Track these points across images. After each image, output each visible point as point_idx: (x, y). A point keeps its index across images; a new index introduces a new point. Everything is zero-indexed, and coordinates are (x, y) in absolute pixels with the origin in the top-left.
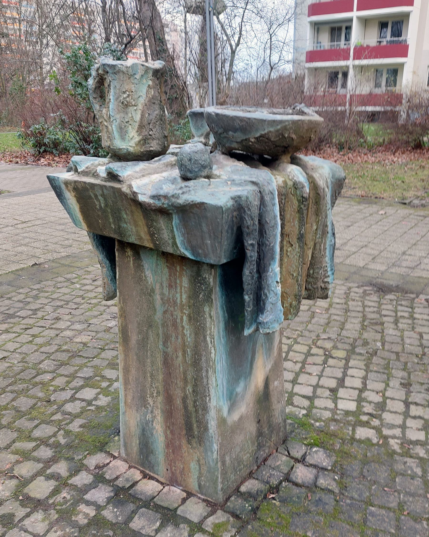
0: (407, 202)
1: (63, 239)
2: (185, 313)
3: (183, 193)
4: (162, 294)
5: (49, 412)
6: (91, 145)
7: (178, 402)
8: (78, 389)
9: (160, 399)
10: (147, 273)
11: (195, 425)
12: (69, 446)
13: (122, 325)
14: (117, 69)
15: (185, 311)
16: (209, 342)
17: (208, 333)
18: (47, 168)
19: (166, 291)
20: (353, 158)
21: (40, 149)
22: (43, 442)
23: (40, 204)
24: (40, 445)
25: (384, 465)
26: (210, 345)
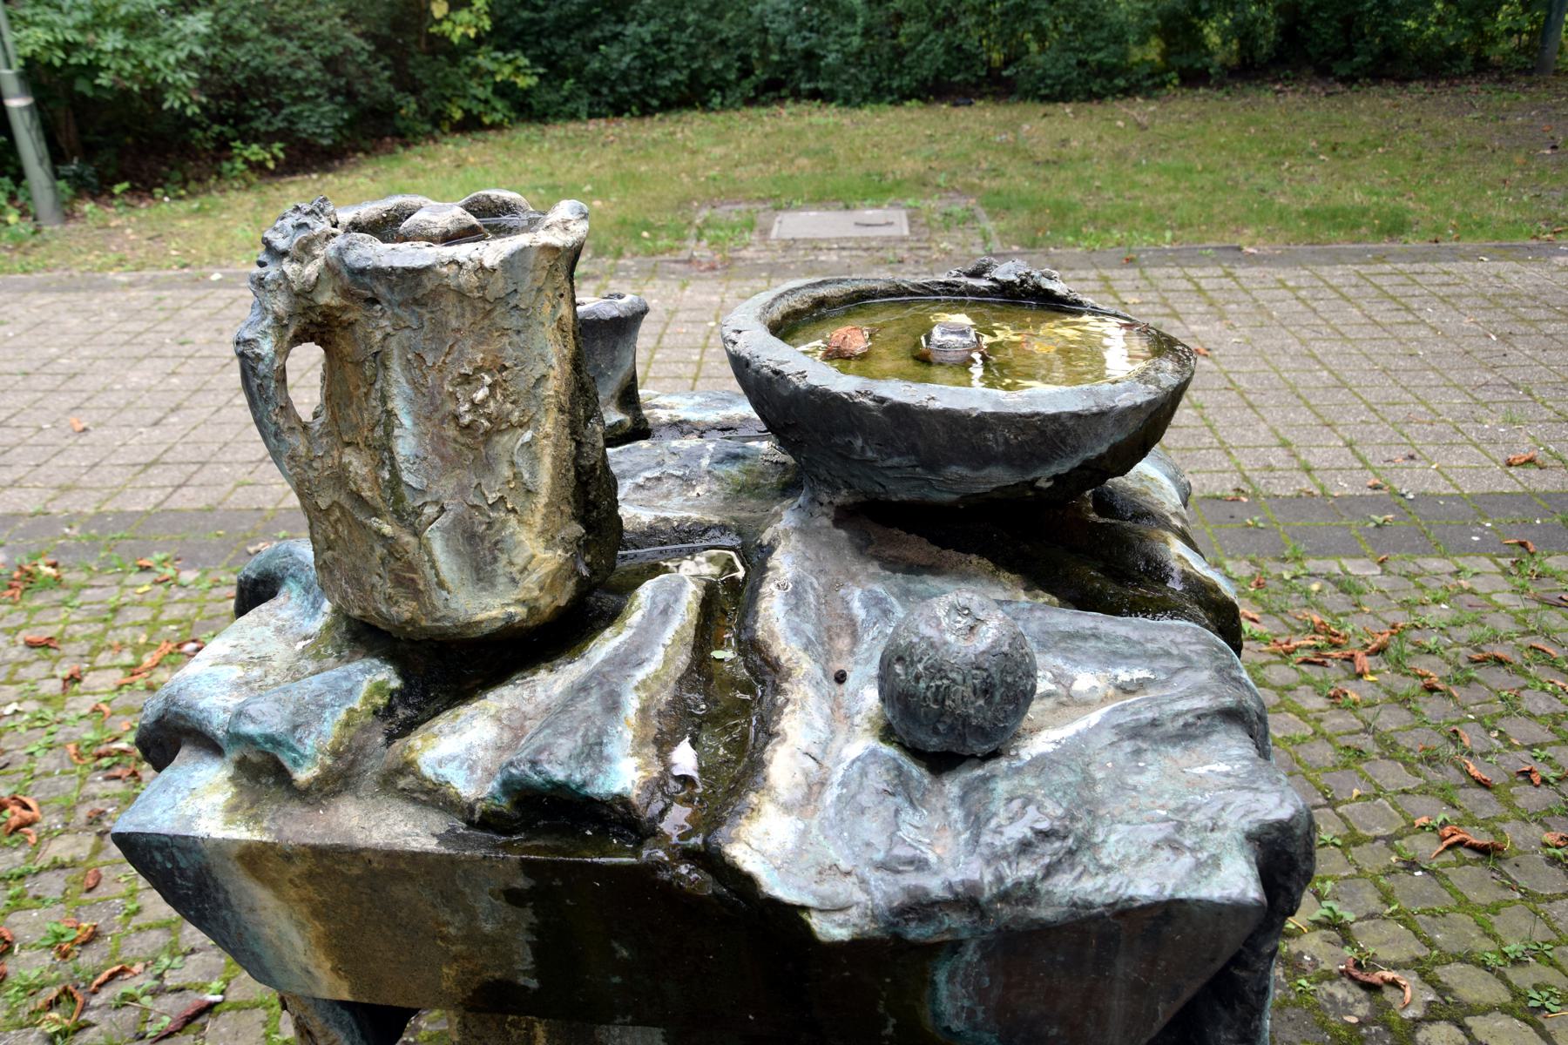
3: (1050, 871)
14: (429, 285)
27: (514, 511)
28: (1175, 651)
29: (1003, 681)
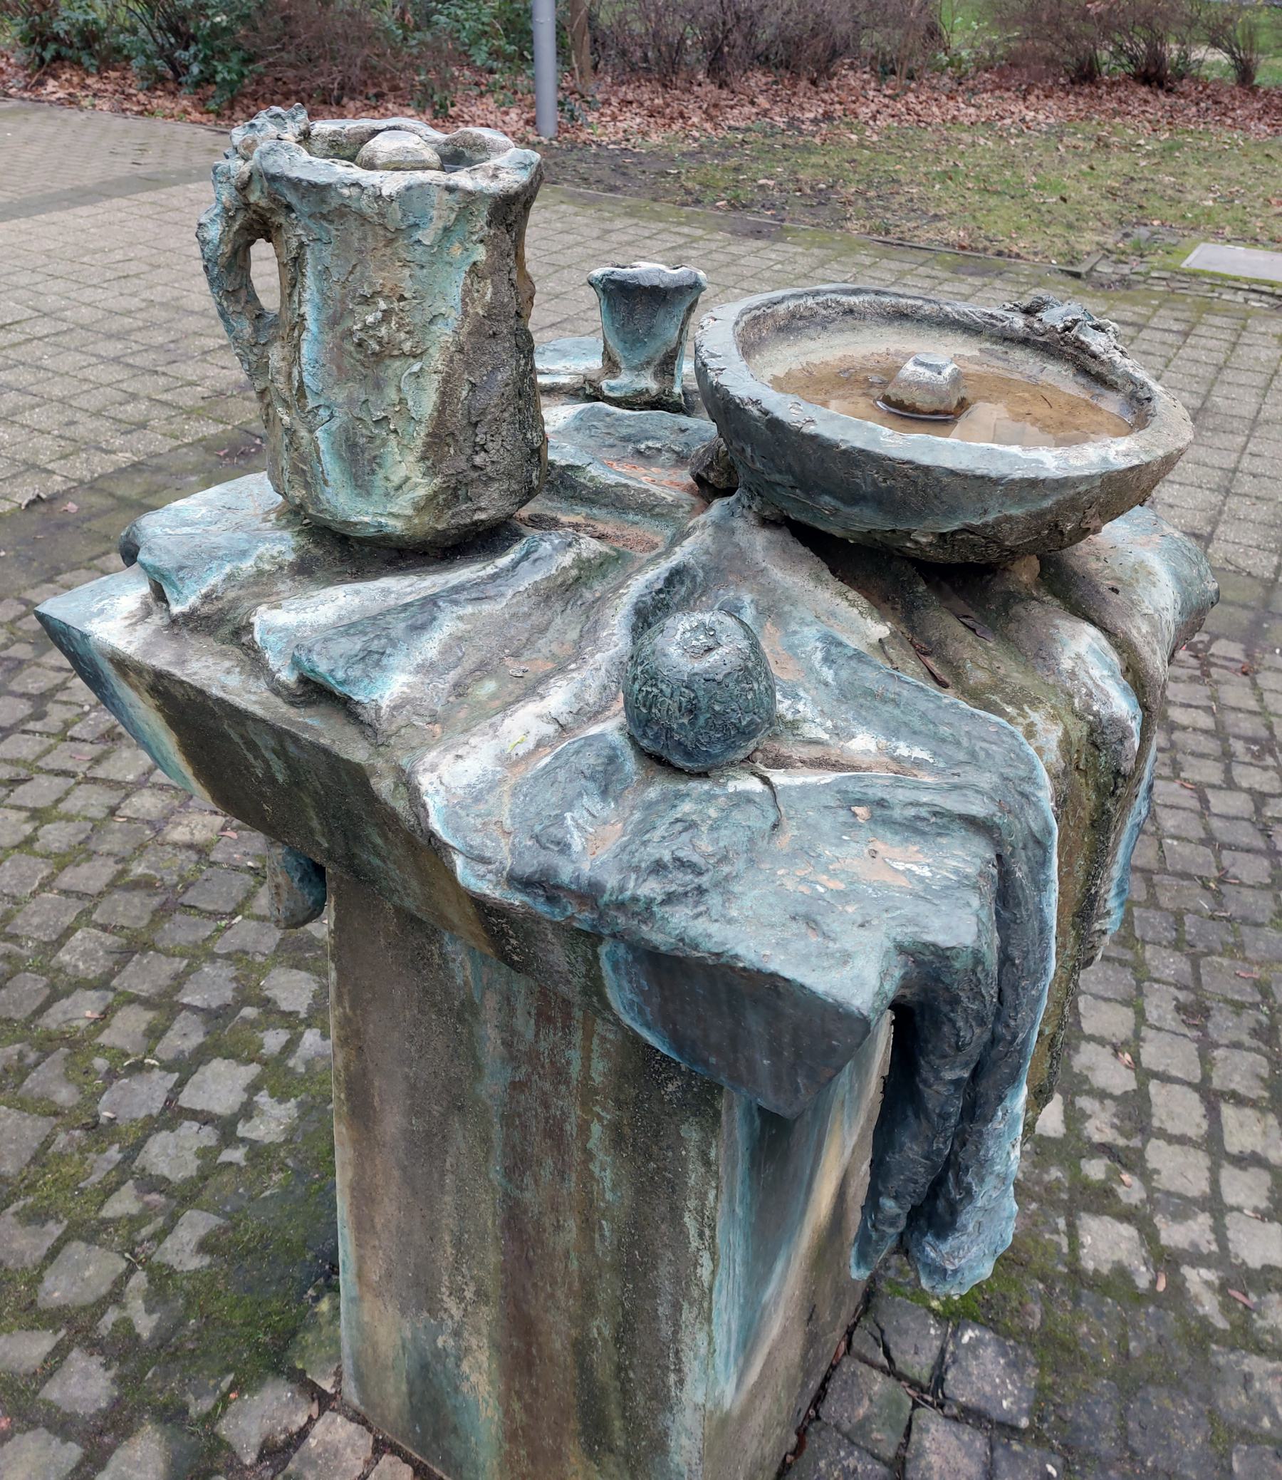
0: (1082, 269)
1: (119, 396)
2: (600, 1119)
3: (670, 899)
4: (509, 1032)
5: (95, 1178)
6: (192, 49)
7: (558, 1344)
8: (186, 1067)
9: (487, 1313)
10: (449, 948)
11: (618, 1424)
12: (166, 1349)
13: (347, 1068)
14: (334, 203)
15: (597, 1109)
16: (693, 1232)
17: (692, 1204)
18: (66, 113)
19: (525, 1026)
20: (918, 108)
21: (44, 49)
22: (76, 1328)
23: (48, 253)
24: (69, 1350)
25: (1187, 1393)
26: (695, 1243)
27: (395, 431)
28: (965, 742)
29: (710, 708)
